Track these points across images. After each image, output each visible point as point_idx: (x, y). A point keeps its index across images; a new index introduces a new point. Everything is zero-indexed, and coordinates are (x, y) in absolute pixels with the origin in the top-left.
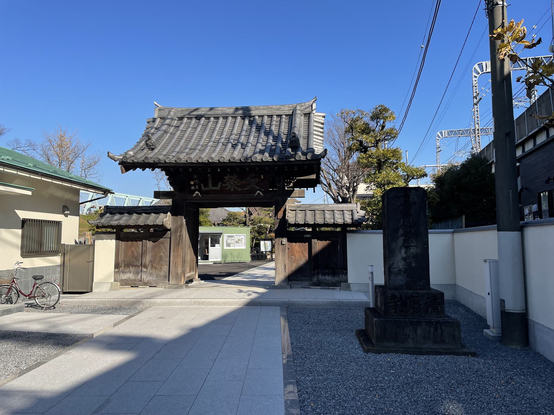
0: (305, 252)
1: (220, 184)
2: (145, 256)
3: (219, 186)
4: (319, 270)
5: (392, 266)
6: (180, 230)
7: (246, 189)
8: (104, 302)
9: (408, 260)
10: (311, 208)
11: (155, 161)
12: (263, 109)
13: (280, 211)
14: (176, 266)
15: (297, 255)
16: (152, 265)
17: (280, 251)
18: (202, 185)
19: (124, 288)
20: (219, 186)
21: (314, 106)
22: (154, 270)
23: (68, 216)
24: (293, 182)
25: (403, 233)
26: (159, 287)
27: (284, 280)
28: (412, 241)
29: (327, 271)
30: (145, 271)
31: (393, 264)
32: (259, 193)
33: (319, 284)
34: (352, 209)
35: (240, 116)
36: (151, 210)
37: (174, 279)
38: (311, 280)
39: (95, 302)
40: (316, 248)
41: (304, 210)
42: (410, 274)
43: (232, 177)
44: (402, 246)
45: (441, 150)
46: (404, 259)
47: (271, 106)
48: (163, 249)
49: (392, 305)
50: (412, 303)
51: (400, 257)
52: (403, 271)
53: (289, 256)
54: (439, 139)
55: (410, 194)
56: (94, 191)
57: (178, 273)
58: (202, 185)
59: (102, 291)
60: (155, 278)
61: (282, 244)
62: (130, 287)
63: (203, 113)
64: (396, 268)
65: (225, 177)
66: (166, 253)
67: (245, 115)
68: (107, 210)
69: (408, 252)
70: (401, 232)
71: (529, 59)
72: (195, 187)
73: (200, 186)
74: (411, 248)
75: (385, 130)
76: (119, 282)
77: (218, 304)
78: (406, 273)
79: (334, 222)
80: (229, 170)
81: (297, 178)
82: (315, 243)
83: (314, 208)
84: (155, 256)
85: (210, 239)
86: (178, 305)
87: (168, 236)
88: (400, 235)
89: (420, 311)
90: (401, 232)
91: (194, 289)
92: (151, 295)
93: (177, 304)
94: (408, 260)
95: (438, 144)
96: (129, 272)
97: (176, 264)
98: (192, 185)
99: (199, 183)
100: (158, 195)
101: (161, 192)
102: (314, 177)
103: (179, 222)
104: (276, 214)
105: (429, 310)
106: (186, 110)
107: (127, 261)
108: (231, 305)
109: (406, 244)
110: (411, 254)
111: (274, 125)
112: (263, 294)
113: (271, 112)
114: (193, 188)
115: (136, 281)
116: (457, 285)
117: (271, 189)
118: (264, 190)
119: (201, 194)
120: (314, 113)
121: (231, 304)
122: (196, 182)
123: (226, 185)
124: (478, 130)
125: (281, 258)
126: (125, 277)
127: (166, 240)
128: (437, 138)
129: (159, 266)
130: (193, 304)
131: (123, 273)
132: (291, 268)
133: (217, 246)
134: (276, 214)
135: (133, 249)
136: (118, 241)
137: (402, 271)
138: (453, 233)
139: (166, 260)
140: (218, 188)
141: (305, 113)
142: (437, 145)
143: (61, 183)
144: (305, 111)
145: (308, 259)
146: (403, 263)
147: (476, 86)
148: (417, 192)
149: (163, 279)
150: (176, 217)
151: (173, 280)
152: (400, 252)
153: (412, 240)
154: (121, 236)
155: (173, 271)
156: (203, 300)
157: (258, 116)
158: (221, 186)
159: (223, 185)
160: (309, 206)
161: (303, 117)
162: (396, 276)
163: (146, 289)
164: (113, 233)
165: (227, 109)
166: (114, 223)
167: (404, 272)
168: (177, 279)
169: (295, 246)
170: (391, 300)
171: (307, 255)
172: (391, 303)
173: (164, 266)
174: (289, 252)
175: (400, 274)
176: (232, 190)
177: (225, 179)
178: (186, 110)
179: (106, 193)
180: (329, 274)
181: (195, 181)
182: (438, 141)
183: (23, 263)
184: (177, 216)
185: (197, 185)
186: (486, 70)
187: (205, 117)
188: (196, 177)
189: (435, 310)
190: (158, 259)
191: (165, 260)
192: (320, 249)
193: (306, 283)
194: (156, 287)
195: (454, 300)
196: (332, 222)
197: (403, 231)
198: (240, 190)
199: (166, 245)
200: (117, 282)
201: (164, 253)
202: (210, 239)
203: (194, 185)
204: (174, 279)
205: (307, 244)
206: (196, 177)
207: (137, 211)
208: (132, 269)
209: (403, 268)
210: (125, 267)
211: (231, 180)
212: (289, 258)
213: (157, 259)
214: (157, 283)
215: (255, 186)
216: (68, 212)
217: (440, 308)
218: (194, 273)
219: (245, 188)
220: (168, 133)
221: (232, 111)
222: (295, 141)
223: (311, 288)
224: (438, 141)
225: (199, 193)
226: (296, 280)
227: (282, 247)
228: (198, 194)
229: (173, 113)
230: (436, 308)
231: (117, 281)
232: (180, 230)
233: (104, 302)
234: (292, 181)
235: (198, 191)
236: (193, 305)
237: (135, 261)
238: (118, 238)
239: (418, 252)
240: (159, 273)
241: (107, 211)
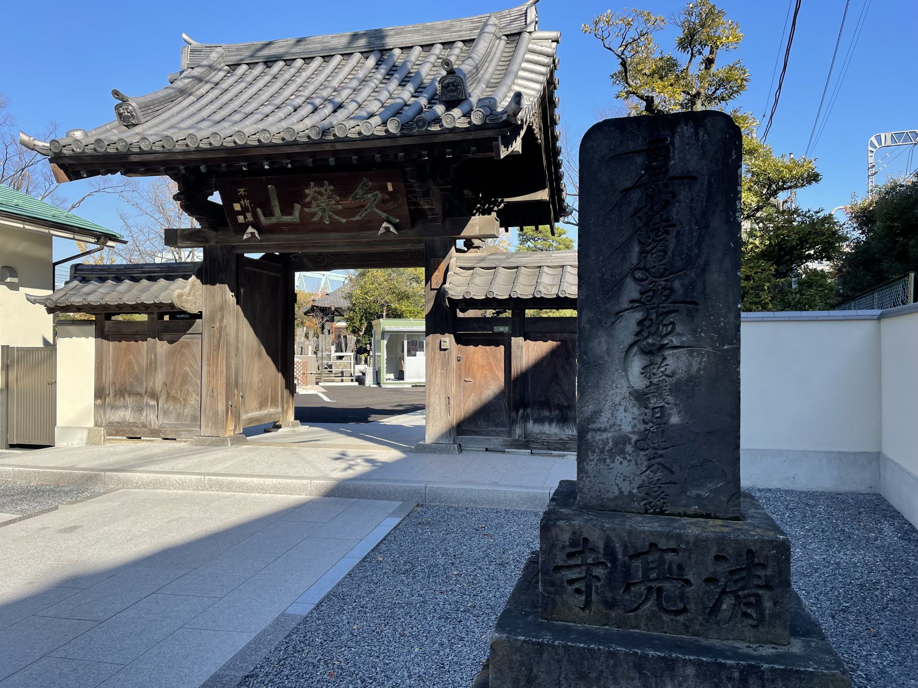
0: (497, 367)
1: (297, 207)
2: (153, 373)
3: (297, 213)
4: (529, 411)
5: (594, 422)
6: (219, 316)
7: (357, 218)
8: (26, 475)
9: (653, 402)
10: (509, 261)
11: (119, 148)
13: (437, 271)
14: (213, 396)
15: (480, 375)
16: (168, 394)
17: (437, 365)
18: (259, 210)
19: (113, 440)
20: (297, 213)
21: (532, 15)
22: (171, 402)
23: (20, 288)
24: (496, 208)
25: (635, 295)
26: (181, 441)
27: (446, 433)
28: (673, 330)
29: (546, 413)
30: (154, 406)
31: (597, 413)
32: (387, 229)
33: (527, 443)
35: (361, 53)
36: (160, 272)
37: (210, 426)
38: (510, 434)
39: (10, 474)
40: (521, 358)
41: (494, 266)
42: (661, 456)
43: (322, 190)
44: (631, 346)
45: (877, 172)
46: (640, 397)
48: (190, 358)
49: (574, 577)
50: (654, 575)
51: (625, 391)
52: (633, 441)
53: (459, 377)
54: (873, 150)
55: (672, 143)
56: (72, 236)
57: (218, 412)
58: (259, 210)
59: (72, 445)
60: (174, 421)
61: (441, 349)
62: (125, 438)
63: (281, 51)
64: (605, 430)
65: (307, 191)
66: (195, 367)
67: (371, 49)
68: (75, 273)
69: (654, 371)
70: (632, 290)
72: (245, 218)
73: (255, 215)
74: (666, 353)
75: (714, 69)
76: (103, 428)
77: (262, 489)
78: (643, 450)
79: (557, 295)
80: (290, 166)
81: (506, 200)
82: (519, 345)
83: (517, 262)
84: (174, 372)
85: (406, 342)
86: (175, 489)
87: (197, 330)
89: (685, 610)
90: (632, 290)
91: (249, 448)
92: (151, 461)
93: (173, 486)
94: (653, 402)
95: (871, 160)
96: (125, 407)
97: (212, 391)
98: (239, 213)
99: (251, 206)
100: (173, 238)
101: (178, 232)
102: (543, 195)
103: (218, 299)
104: (428, 278)
105: (724, 607)
106: (247, 48)
107: (120, 383)
108: (292, 494)
109: (650, 341)
110: (667, 376)
111: (431, 62)
112: (385, 465)
113: (430, 37)
115: (137, 427)
116: (884, 455)
118: (398, 220)
119: (260, 233)
120: (530, 33)
121: (291, 490)
122: (245, 205)
123: (312, 210)
125: (438, 381)
126: (118, 416)
127: (194, 338)
128: (870, 148)
129: (181, 394)
130: (207, 486)
131: (112, 408)
132: (465, 405)
133: (420, 355)
134: (428, 278)
135: (130, 358)
136: (100, 339)
137: (630, 443)
138: (880, 318)
139: (195, 382)
140: (295, 217)
141: (509, 33)
142: (869, 162)
143: (21, 226)
144: (509, 29)
145: (503, 384)
146: (636, 411)
148: (701, 133)
149: (189, 422)
150: (212, 287)
151: (207, 426)
152: (625, 370)
153: (672, 323)
154: (106, 329)
155: (208, 406)
156: (230, 478)
157: (401, 48)
158: (301, 212)
159: (306, 210)
160: (504, 257)
161: (503, 43)
162: (605, 460)
163: (155, 444)
164: (88, 322)
165: (332, 37)
166: (93, 299)
167: (638, 447)
168: (215, 424)
169: (475, 353)
170: (570, 555)
171: (502, 380)
172: (569, 567)
173: (192, 396)
174: (459, 368)
175: (622, 452)
176: (327, 223)
177: (307, 195)
178: (247, 48)
179: (102, 240)
180: (551, 421)
181: (242, 202)
182: (872, 155)
184: (213, 284)
185: (249, 211)
187: (284, 61)
188: (242, 191)
189: (749, 611)
190: (179, 380)
191: (193, 382)
192: (530, 361)
193: (497, 441)
194: (175, 439)
195: (874, 495)
196: (552, 293)
197: (638, 288)
198: (344, 221)
199: (194, 349)
200: (100, 428)
201: (191, 366)
202: (406, 342)
203: (243, 212)
204: (210, 426)
205: (502, 348)
206: (242, 191)
207: (134, 275)
208: (129, 400)
209: (633, 433)
210: (115, 396)
211: (319, 197)
212: (460, 382)
213: (177, 379)
214: (177, 432)
215: (377, 211)
216: (15, 280)
217: (768, 604)
218: (280, 409)
219: (355, 216)
220: (190, 94)
221: (344, 41)
222: (454, 86)
223: (508, 452)
224: (872, 155)
225: (256, 232)
226: (476, 433)
227: (442, 356)
228: (252, 234)
229: (217, 56)
230: (753, 600)
231: (99, 426)
232: (219, 316)
233: (26, 475)
234: (493, 208)
235: (254, 227)
236: (207, 490)
237: (135, 383)
238: (101, 334)
239: (695, 366)
240: (182, 410)
241: (76, 275)
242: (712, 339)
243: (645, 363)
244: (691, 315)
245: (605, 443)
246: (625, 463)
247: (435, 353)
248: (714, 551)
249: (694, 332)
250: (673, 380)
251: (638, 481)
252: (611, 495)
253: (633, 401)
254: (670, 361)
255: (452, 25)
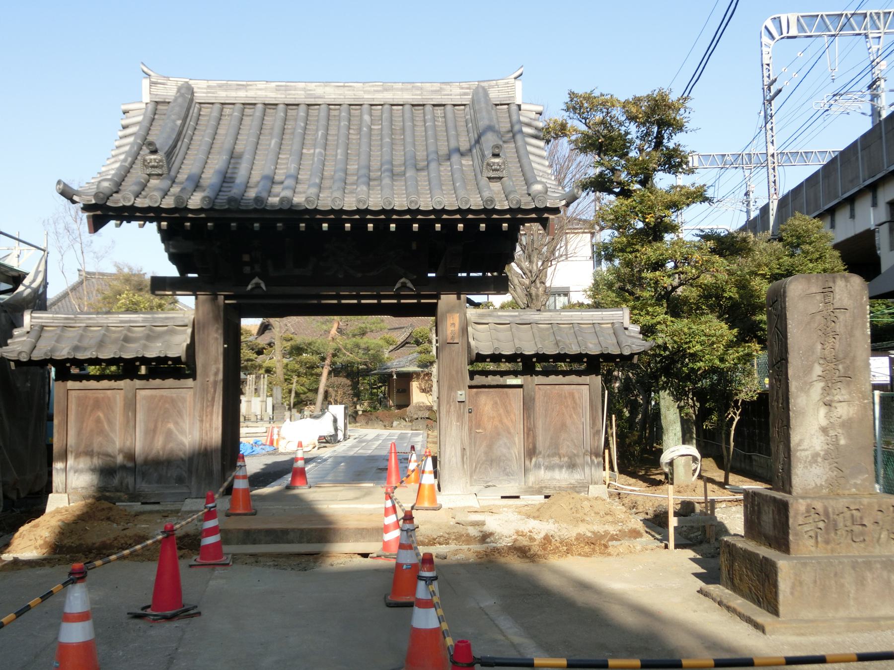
4: (541, 460)
9: (832, 433)
12: (402, 90)
25: (820, 373)
29: (556, 460)
34: (612, 321)
41: (508, 322)
46: (824, 430)
47: (419, 84)
51: (816, 427)
64: (806, 450)
71: (871, 13)
88: (814, 377)
90: (818, 370)
114: (247, 270)
117: (461, 272)
124: (773, 155)
147: (768, 65)
162: (807, 467)
175: (816, 462)
183: (503, 497)
186: (788, 33)
197: (822, 369)
198: (359, 275)
209: (822, 450)
222: (155, 162)
235: (260, 279)
239: (851, 412)
242: (859, 398)
243: (826, 411)
244: (848, 384)
245: (807, 457)
246: (818, 468)
247: (450, 406)
248: (876, 508)
249: (850, 393)
250: (840, 420)
251: (825, 477)
252: (811, 487)
253: (821, 433)
254: (839, 409)
255: (441, 88)
